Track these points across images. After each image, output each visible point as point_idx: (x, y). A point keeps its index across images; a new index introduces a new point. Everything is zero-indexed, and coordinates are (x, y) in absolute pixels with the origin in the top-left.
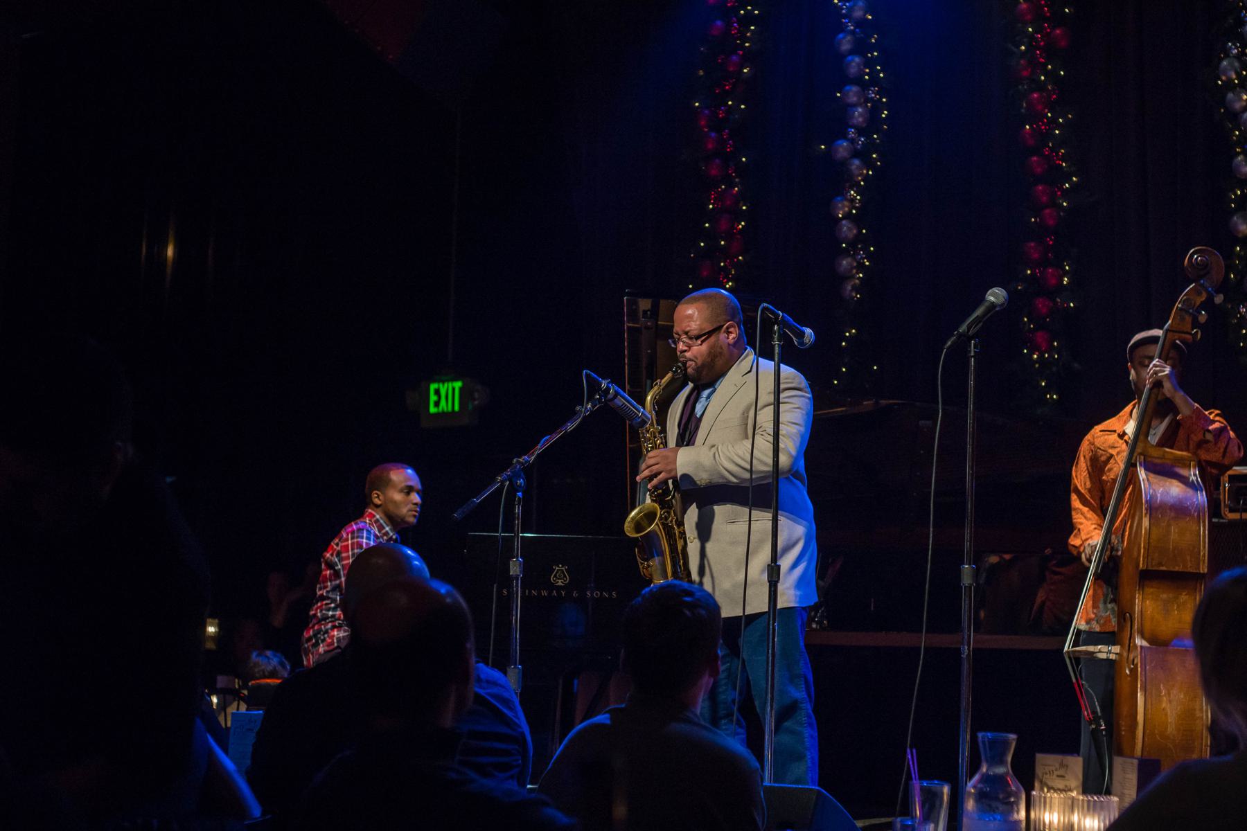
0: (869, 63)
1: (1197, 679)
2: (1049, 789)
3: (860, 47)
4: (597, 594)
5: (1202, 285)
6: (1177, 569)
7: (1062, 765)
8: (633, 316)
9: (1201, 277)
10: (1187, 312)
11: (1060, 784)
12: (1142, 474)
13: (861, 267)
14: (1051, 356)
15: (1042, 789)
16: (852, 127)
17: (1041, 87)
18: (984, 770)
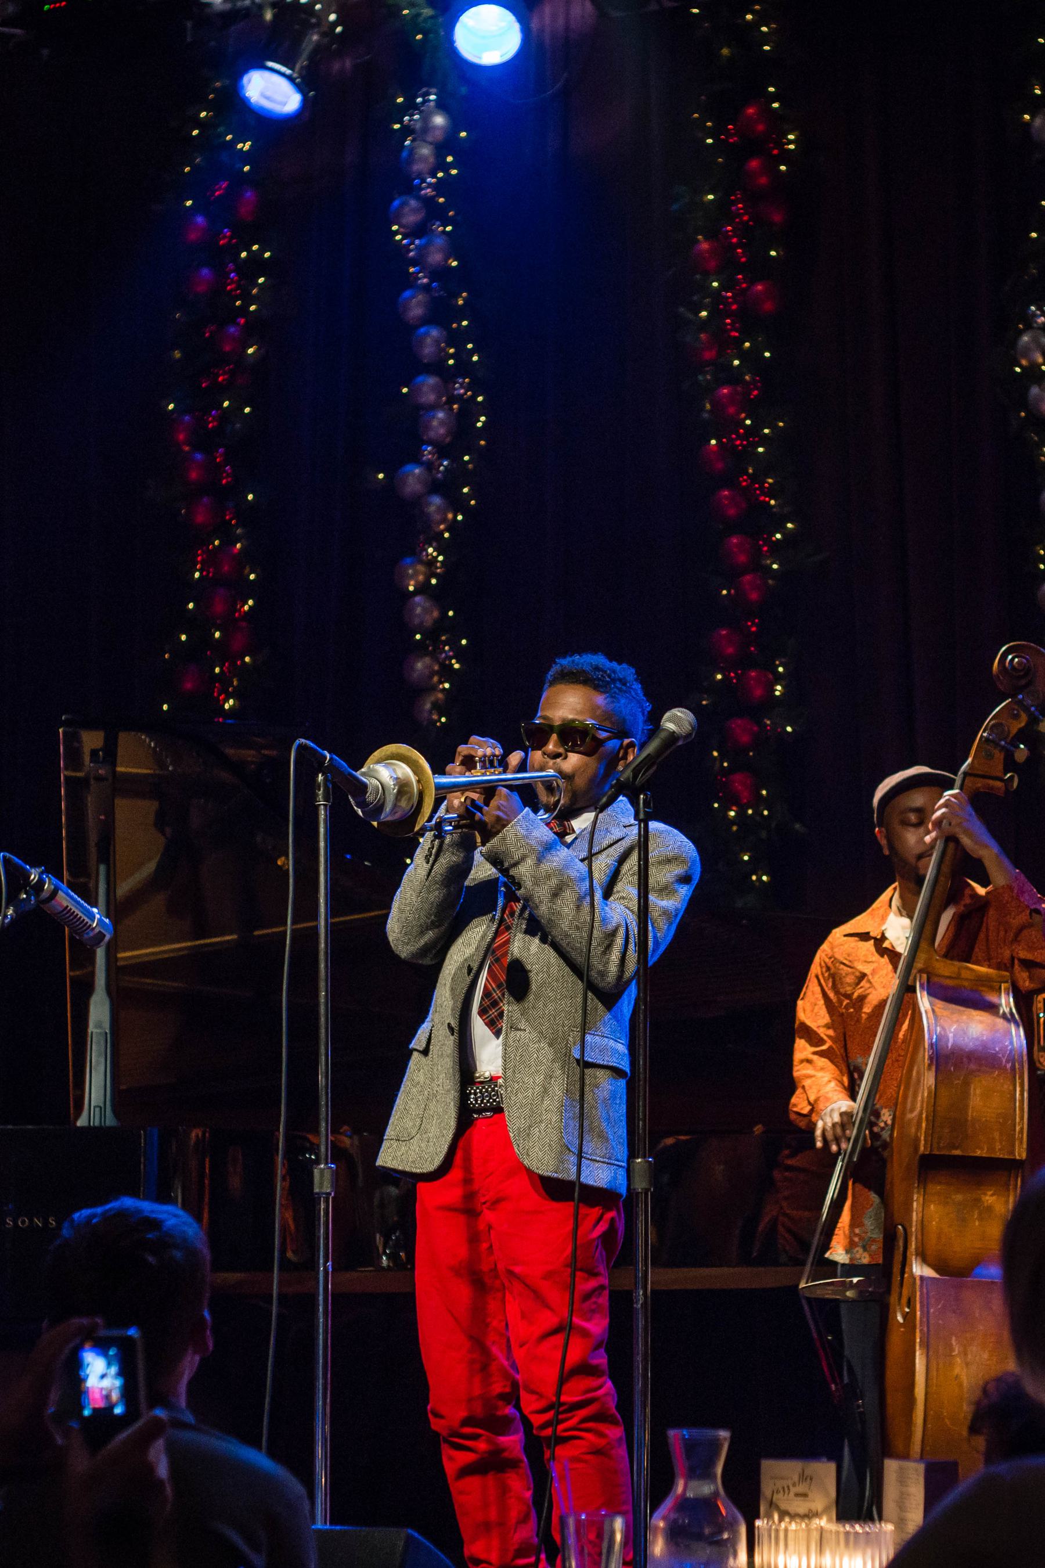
0: (456, 338)
1: (1006, 1335)
2: (783, 1514)
3: (440, 313)
4: (23, 1222)
5: (1020, 703)
6: (978, 1153)
7: (803, 1477)
8: (74, 758)
9: (1020, 689)
10: (996, 744)
11: (800, 1506)
12: (924, 1002)
13: (446, 672)
14: (758, 813)
15: (769, 1516)
16: (430, 443)
17: (733, 377)
18: (680, 1488)
